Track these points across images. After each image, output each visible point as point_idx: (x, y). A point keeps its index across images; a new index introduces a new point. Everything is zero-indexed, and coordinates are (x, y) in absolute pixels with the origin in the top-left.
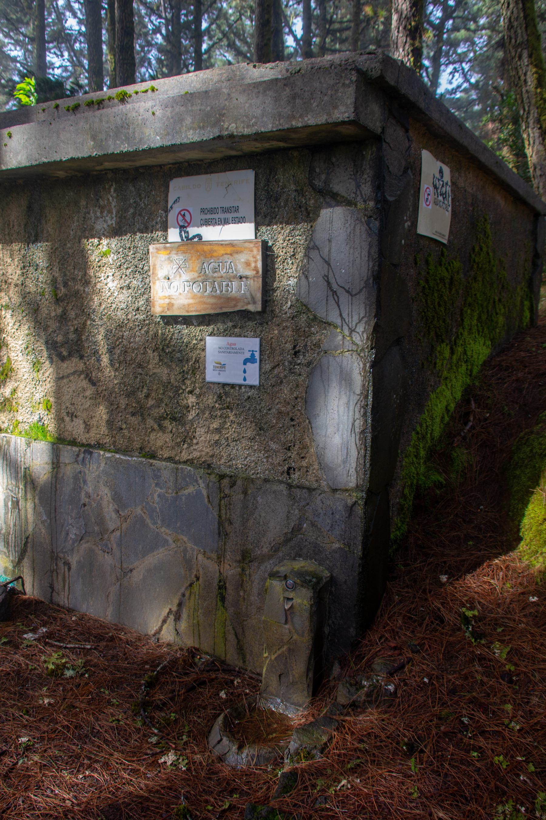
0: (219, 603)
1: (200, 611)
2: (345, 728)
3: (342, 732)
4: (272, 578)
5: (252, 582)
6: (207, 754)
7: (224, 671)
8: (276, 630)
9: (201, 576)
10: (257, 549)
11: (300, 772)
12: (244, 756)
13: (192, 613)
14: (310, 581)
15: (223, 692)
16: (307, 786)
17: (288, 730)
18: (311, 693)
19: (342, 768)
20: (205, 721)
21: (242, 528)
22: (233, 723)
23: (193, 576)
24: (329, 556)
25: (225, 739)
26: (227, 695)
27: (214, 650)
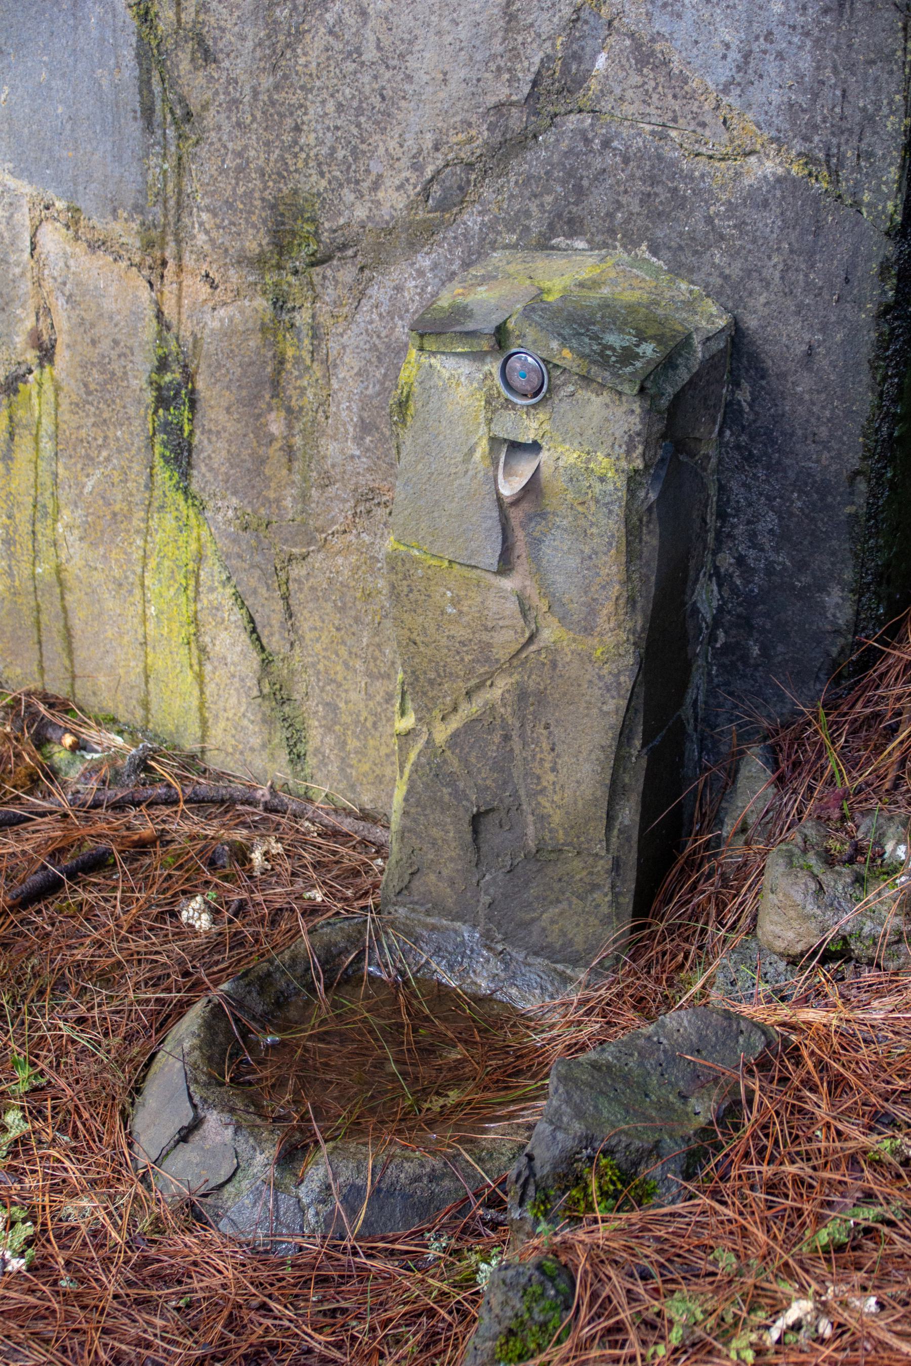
0: (164, 476)
1: (66, 515)
2: (798, 1061)
3: (784, 1080)
4: (431, 344)
5: (329, 367)
6: (128, 1190)
7: (198, 802)
8: (456, 601)
9: (62, 340)
10: (349, 196)
11: (583, 1263)
12: (306, 1192)
13: (25, 528)
14: (628, 356)
15: (197, 902)
16: (619, 1328)
17: (518, 1073)
18: (627, 901)
19: (790, 1243)
20: (115, 1041)
21: (267, 81)
22: (252, 1047)
23: (20, 340)
24: (727, 227)
25: (213, 1119)
26: (215, 913)
27: (146, 706)
